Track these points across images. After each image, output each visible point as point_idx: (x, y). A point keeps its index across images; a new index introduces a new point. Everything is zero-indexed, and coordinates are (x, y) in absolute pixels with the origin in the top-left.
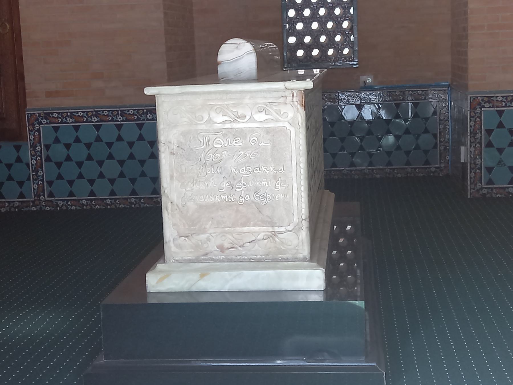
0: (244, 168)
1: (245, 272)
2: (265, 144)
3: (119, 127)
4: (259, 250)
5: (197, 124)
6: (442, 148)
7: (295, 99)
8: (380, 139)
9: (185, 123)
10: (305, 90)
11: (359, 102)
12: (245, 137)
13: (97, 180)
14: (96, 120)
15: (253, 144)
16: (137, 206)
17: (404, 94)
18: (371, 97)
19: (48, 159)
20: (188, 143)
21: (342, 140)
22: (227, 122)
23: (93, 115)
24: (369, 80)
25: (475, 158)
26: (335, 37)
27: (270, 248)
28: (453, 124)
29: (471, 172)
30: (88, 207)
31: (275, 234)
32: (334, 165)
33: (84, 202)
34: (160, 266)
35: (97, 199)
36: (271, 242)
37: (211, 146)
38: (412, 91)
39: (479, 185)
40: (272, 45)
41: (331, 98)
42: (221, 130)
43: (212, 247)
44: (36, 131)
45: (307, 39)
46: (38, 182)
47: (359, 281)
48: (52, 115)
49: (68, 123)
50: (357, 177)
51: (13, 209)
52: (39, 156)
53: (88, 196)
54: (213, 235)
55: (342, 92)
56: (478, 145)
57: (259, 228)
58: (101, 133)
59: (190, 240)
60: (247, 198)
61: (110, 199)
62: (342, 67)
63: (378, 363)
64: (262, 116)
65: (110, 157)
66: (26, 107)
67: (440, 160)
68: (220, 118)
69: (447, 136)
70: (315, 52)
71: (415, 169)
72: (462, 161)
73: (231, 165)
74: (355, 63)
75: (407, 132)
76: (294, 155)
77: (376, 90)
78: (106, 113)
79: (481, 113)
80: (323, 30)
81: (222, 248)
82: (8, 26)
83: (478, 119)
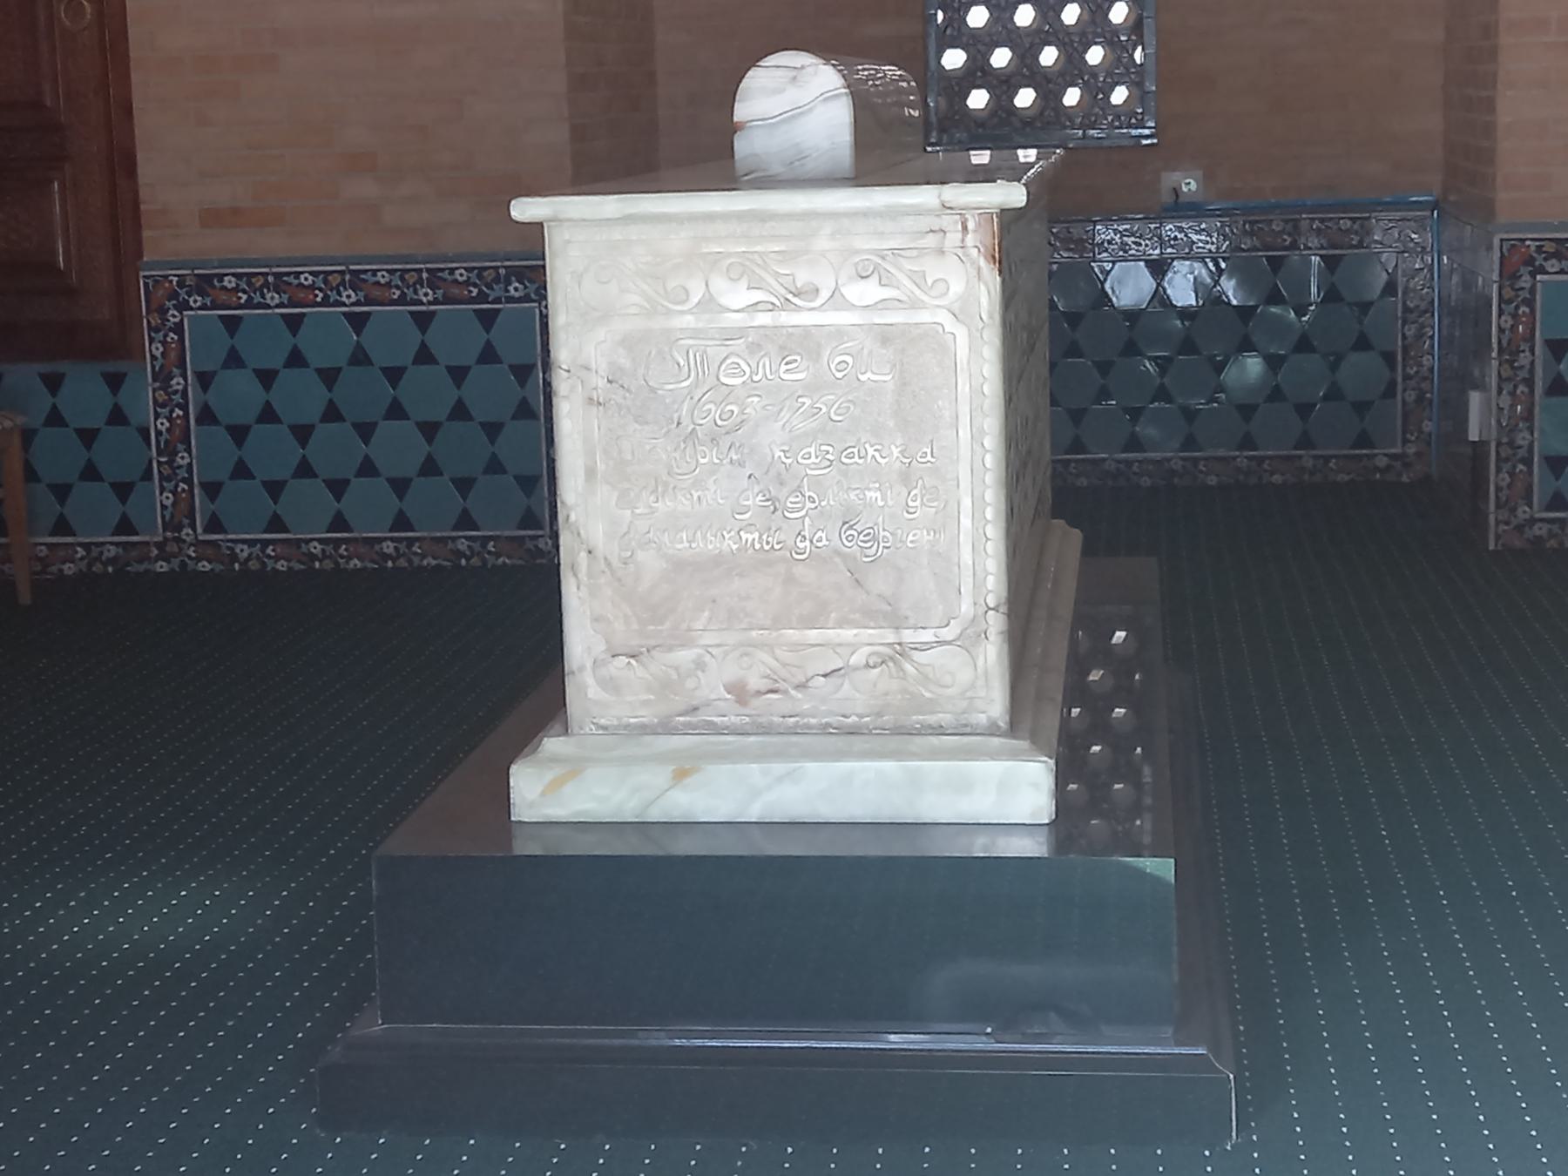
0: (812, 450)
1: (812, 767)
2: (879, 376)
3: (423, 321)
4: (854, 699)
5: (668, 312)
6: (1411, 396)
7: (970, 239)
8: (1219, 368)
9: (633, 310)
10: (1003, 210)
11: (1157, 251)
12: (814, 354)
13: (319, 480)
14: (354, 299)
15: (839, 375)
16: (475, 561)
17: (1296, 227)
18: (1194, 237)
19: (207, 416)
20: (641, 371)
21: (1104, 368)
22: (760, 307)
23: (343, 283)
24: (1190, 186)
25: (1513, 429)
26: (1085, 51)
27: (886, 694)
28: (1446, 321)
29: (1498, 470)
30: (329, 565)
32: (1077, 446)
33: (316, 549)
34: (552, 744)
35: (355, 540)
36: (891, 676)
37: (711, 381)
38: (1322, 221)
39: (1523, 512)
40: (892, 71)
41: (1071, 240)
42: (742, 332)
43: (711, 687)
44: (171, 329)
45: (1001, 58)
46: (177, 486)
47: (1148, 801)
48: (221, 281)
49: (269, 307)
50: (1146, 482)
51: (97, 568)
52: (179, 406)
53: (265, 532)
55: (1107, 220)
56: (1521, 388)
57: (855, 631)
58: (369, 337)
59: (644, 665)
60: (820, 540)
61: (392, 539)
62: (1106, 143)
63: (1215, 1048)
64: (869, 292)
65: (396, 411)
66: (140, 256)
67: (1404, 433)
68: (737, 296)
69: (1426, 360)
70: (1025, 98)
71: (1327, 459)
72: (1473, 436)
74: (1147, 132)
75: (1304, 344)
76: (964, 410)
77: (1212, 214)
78: (383, 278)
79: (1532, 290)
81: (739, 692)
83: (1524, 309)
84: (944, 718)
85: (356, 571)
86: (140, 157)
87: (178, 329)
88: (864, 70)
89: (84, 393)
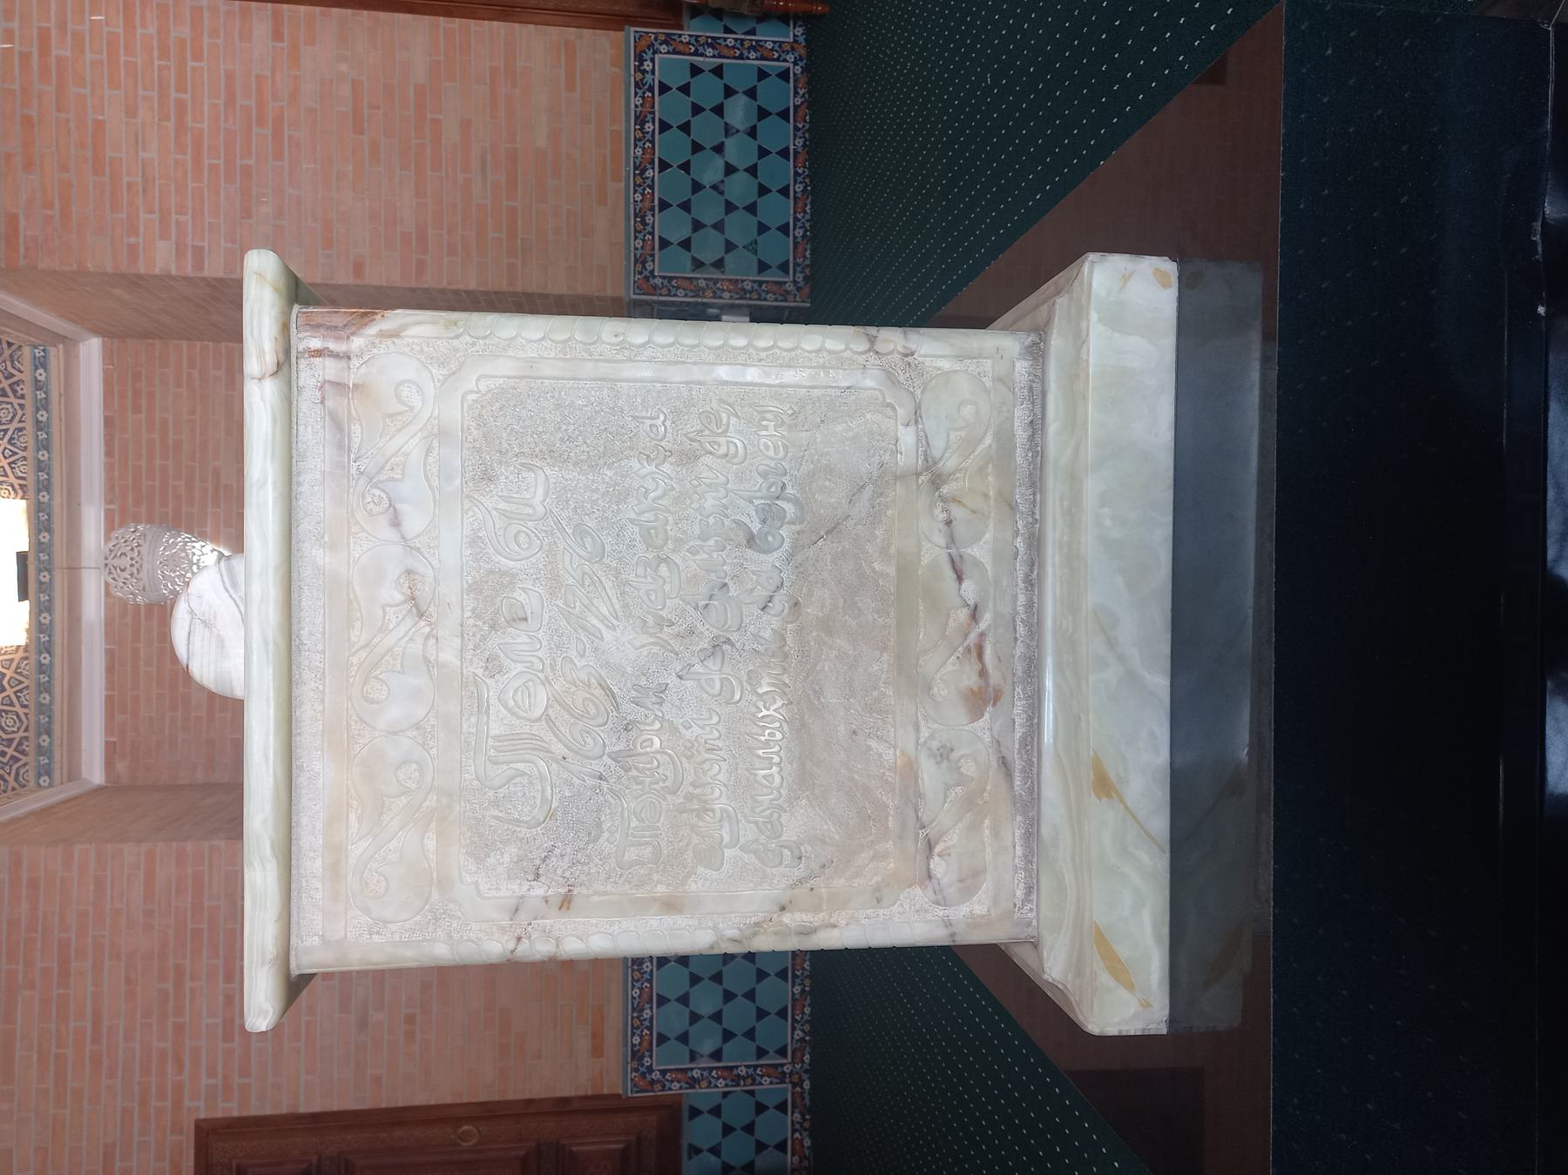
20: (523, 831)
30: (807, 982)
33: (798, 989)
39: (790, 287)
43: (976, 738)
51: (806, 1125)
54: (925, 733)
59: (942, 834)
66: (619, 1095)
73: (627, 645)
81: (980, 699)
82: (465, 1128)
84: (1020, 415)
85: (812, 966)
86: (559, 1094)
87: (664, 1072)
89: (700, 1132)
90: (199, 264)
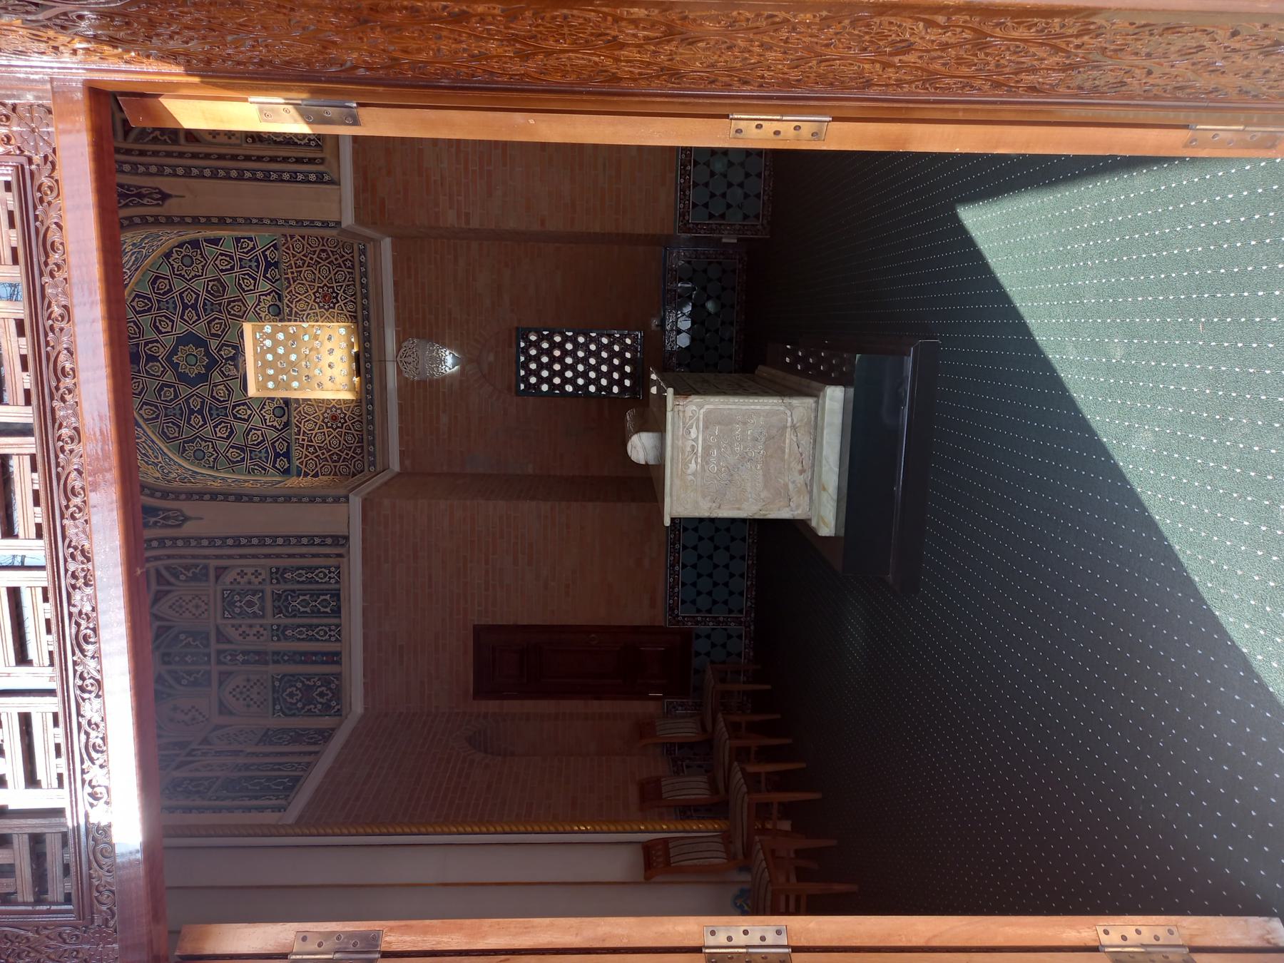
4: (806, 440)
8: (709, 314)
19: (709, 611)
31: (794, 427)
34: (814, 524)
42: (702, 466)
43: (800, 479)
45: (616, 376)
64: (693, 431)
65: (710, 557)
68: (693, 466)
75: (704, 289)
80: (609, 361)
81: (802, 472)
84: (813, 416)
88: (629, 425)
89: (701, 645)
90: (467, 222)
